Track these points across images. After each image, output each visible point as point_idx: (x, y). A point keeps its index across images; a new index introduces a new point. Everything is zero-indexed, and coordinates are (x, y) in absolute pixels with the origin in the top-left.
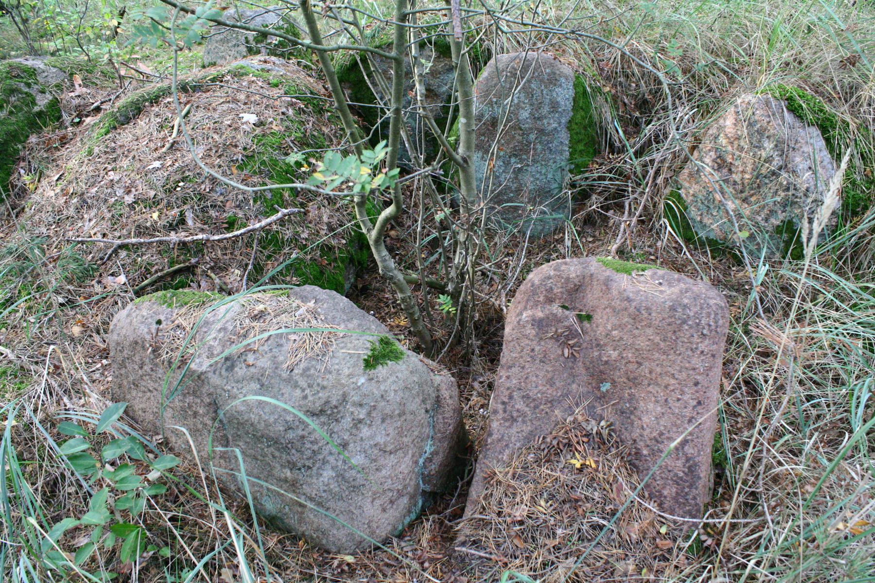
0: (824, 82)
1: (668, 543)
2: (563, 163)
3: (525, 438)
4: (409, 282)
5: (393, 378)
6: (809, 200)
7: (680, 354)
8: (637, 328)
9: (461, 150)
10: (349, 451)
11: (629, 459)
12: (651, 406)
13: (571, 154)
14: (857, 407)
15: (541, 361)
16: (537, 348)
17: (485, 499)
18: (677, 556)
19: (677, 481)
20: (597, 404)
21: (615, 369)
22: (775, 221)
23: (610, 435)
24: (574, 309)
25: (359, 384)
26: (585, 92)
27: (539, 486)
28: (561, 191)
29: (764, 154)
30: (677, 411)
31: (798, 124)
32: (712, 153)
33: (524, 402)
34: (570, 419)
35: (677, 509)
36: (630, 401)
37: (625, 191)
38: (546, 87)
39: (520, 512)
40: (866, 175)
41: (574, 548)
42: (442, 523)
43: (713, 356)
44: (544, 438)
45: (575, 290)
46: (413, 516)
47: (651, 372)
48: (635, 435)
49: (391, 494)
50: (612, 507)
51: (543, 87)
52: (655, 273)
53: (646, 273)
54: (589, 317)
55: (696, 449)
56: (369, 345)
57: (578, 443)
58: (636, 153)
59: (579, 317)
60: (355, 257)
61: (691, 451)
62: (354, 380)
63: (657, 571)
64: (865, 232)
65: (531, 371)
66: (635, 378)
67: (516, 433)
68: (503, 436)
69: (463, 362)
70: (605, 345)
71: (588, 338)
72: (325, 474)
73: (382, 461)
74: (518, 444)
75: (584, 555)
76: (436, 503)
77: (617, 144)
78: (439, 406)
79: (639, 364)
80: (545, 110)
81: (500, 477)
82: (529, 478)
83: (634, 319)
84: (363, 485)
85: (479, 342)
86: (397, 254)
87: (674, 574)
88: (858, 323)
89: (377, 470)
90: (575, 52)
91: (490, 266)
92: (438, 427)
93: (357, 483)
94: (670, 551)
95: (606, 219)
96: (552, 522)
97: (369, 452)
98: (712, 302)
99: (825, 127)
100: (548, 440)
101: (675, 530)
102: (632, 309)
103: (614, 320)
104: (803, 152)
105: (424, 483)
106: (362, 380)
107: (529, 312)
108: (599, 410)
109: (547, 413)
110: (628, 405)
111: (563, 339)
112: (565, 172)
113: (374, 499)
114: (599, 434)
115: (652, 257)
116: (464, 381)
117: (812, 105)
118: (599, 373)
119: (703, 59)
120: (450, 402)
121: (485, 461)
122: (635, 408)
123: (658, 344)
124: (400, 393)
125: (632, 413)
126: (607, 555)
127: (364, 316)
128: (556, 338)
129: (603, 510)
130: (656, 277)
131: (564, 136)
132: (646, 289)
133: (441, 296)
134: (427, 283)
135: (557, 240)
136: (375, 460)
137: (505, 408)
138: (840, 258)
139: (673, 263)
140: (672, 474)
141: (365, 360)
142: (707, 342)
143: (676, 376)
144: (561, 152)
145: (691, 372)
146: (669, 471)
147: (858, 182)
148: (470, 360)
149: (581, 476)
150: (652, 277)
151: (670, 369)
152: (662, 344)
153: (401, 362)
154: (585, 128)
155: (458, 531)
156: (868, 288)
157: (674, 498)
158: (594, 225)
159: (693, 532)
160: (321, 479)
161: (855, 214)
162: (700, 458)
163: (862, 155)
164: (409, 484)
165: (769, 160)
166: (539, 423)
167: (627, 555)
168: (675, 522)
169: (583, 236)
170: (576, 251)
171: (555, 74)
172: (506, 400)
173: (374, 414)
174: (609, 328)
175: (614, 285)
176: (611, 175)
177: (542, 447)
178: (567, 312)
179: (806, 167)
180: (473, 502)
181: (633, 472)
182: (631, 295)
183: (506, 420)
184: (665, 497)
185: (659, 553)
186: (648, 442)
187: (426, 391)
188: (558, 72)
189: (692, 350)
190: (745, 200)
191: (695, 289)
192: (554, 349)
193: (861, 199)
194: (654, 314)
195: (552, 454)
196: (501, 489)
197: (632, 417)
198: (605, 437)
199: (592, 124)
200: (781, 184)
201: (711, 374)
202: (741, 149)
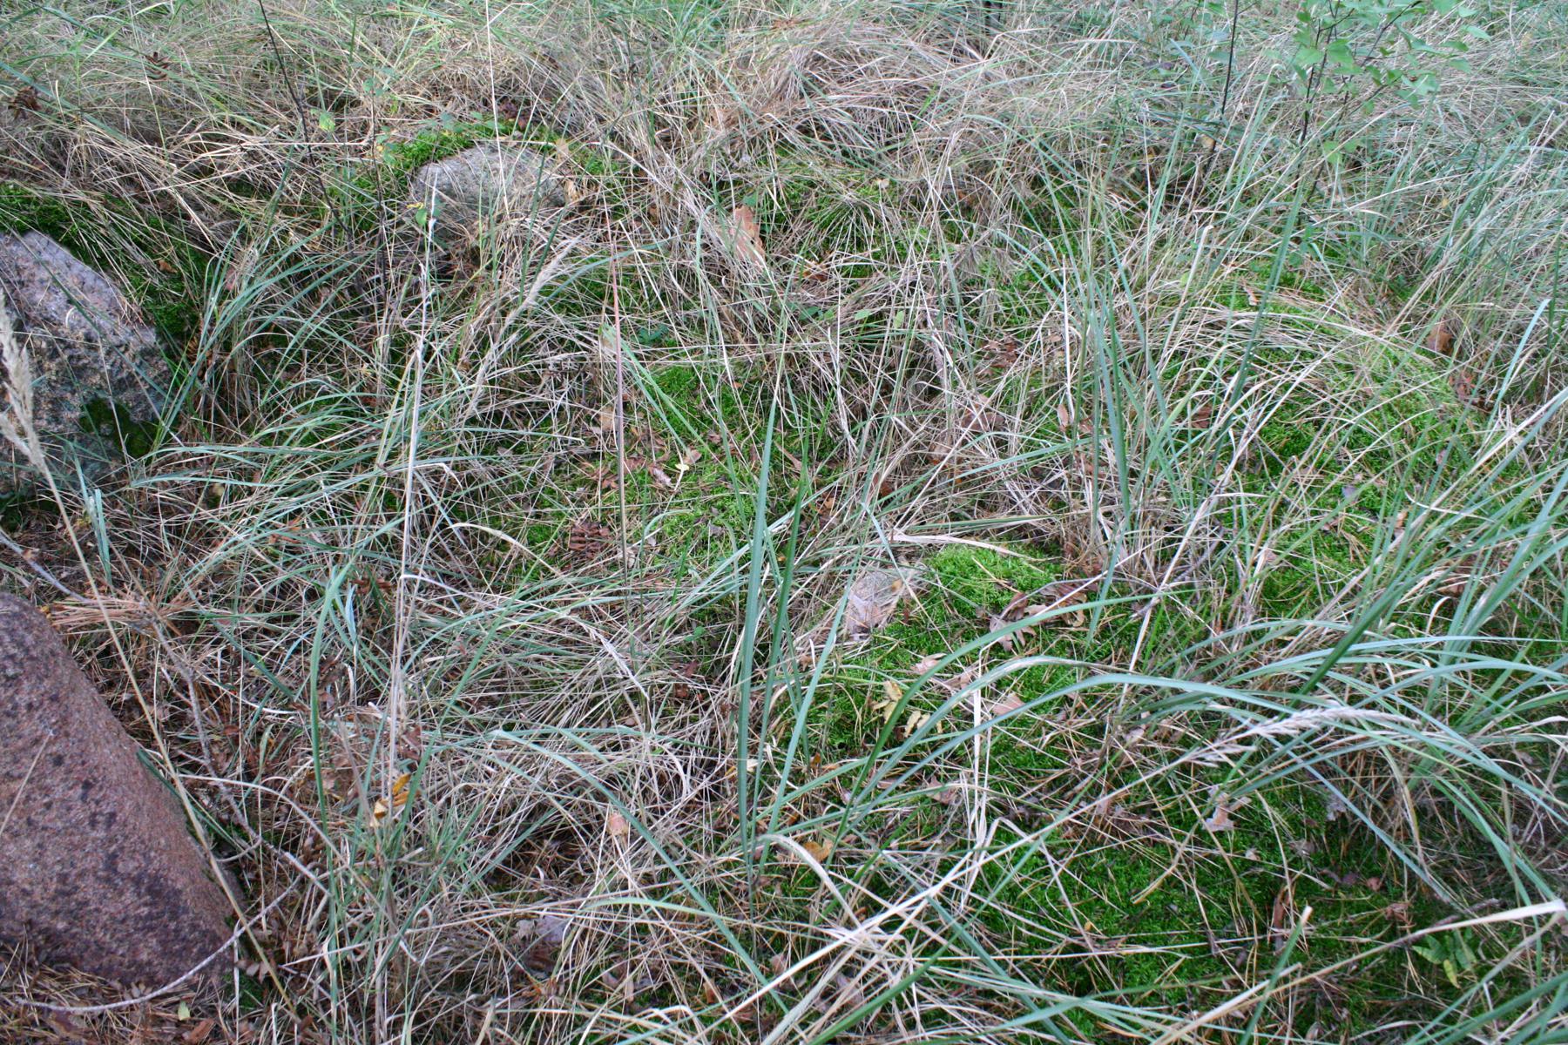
1: (206, 1024)
6: (102, 353)
11: (43, 957)
14: (1446, 297)
18: (234, 1030)
22: (72, 414)
30: (60, 824)
43: (54, 699)
48: (23, 912)
55: (137, 856)
61: (132, 865)
64: (216, 357)
99: (52, 223)
101: (202, 996)
104: (42, 281)
138: (207, 417)
140: (131, 923)
142: (26, 685)
143: (16, 773)
146: (123, 921)
147: (160, 287)
156: (271, 435)
157: (164, 954)
161: (183, 336)
162: (156, 864)
163: (139, 244)
168: (192, 986)
179: (62, 303)
181: (66, 971)
184: (149, 963)
186: (53, 907)
189: (8, 714)
193: (179, 311)
200: (39, 351)
201: (72, 729)
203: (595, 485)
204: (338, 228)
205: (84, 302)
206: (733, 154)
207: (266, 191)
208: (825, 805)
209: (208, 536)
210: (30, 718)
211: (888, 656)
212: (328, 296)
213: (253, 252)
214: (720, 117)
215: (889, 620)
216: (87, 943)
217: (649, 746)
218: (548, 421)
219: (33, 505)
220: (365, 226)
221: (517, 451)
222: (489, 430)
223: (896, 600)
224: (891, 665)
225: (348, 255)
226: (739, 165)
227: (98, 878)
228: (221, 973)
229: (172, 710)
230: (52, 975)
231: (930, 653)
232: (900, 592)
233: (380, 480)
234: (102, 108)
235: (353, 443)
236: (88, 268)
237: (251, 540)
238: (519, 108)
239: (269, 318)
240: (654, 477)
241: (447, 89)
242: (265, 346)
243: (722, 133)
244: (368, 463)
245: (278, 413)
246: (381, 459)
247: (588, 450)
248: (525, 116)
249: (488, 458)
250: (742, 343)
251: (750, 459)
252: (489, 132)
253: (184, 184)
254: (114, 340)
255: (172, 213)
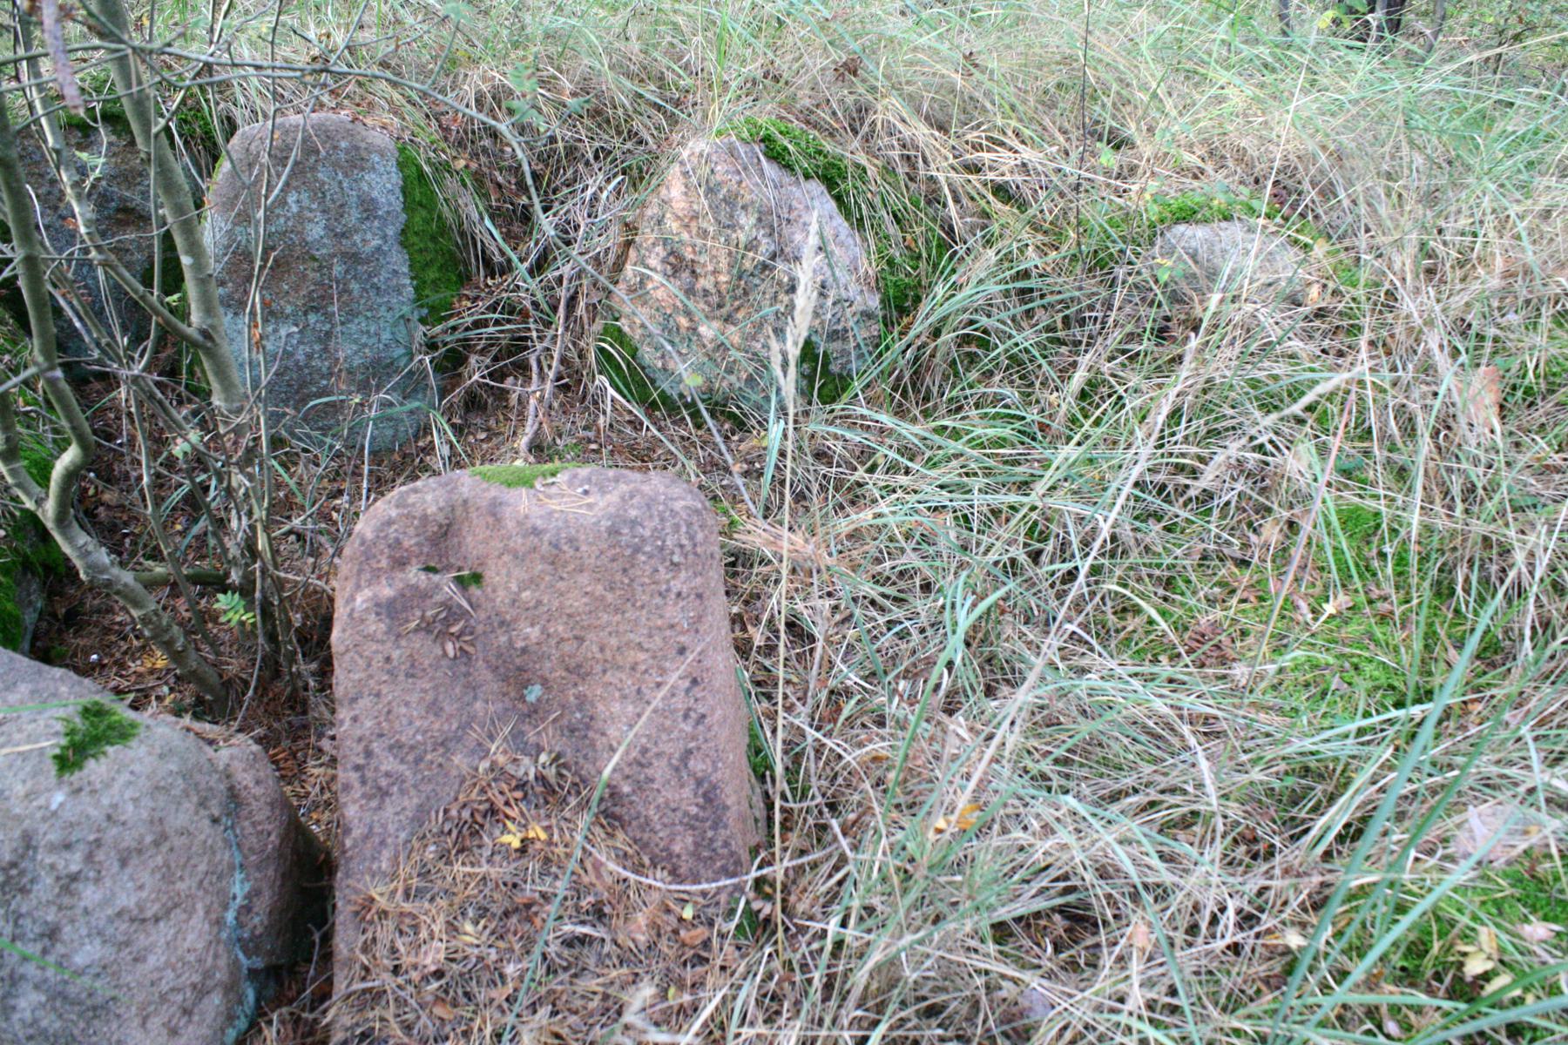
0: (818, 106)
1: (701, 932)
2: (406, 309)
3: (412, 820)
4: (151, 585)
5: (125, 777)
7: (642, 607)
8: (562, 578)
9: (195, 317)
10: (63, 942)
12: (616, 707)
13: (416, 289)
15: (408, 675)
16: (395, 654)
17: (365, 950)
19: (691, 823)
20: (526, 728)
21: (541, 658)
23: (560, 775)
24: (448, 568)
25: (54, 807)
26: (421, 175)
27: (457, 900)
28: (411, 359)
29: (743, 238)
31: (787, 179)
32: (659, 249)
33: (395, 757)
34: (484, 765)
35: (702, 871)
36: (580, 708)
37: (526, 339)
38: (346, 175)
39: (432, 957)
40: (908, 248)
41: (543, 990)
42: (297, 1020)
43: (699, 596)
44: (446, 811)
45: (441, 538)
46: (242, 1024)
47: (602, 650)
49: (180, 997)
50: (591, 899)
51: (340, 177)
52: (575, 476)
53: (560, 478)
54: (477, 578)
56: (59, 727)
57: (507, 803)
58: (531, 272)
59: (459, 581)
60: (34, 559)
61: (701, 766)
62: (41, 801)
63: (693, 985)
64: (923, 338)
65: (394, 698)
66: (579, 666)
67: (394, 815)
68: (371, 828)
69: (292, 708)
70: (515, 620)
71: (483, 615)
72: (22, 1003)
73: (142, 941)
74: (403, 835)
75: (564, 998)
76: (282, 985)
77: (497, 258)
78: (238, 805)
79: (580, 639)
80: (353, 216)
81: (382, 902)
82: (436, 890)
83: (553, 563)
84: (114, 999)
85: (314, 666)
86: (126, 535)
87: (721, 981)
88: (942, 487)
89: (136, 960)
90: (390, 102)
91: (304, 523)
92: (247, 845)
93: (99, 1000)
94: (706, 944)
95: (503, 395)
96: (493, 955)
97: (110, 930)
98: (678, 505)
99: (831, 176)
100: (454, 813)
102: (545, 548)
103: (520, 573)
105: (248, 955)
106: (59, 798)
107: (367, 593)
108: (531, 736)
109: (440, 765)
110: (578, 715)
111: (438, 626)
112: (412, 325)
113: (145, 1020)
114: (541, 778)
115: (594, 446)
116: (301, 743)
117: (803, 144)
118: (516, 673)
119: (619, 89)
120: (258, 791)
121: (350, 882)
122: (592, 718)
123: (603, 598)
124: (147, 802)
125: (588, 727)
126: (603, 985)
127: (40, 672)
128: (426, 627)
129: (578, 909)
130: (577, 482)
131: (398, 260)
132: (562, 507)
133: (220, 596)
134: (188, 578)
135: (423, 449)
136: (127, 944)
137: (363, 776)
138: (895, 389)
139: (632, 448)
140: (679, 814)
141: (55, 757)
142: (683, 575)
143: (646, 646)
144: (398, 290)
145: (668, 633)
146: (674, 810)
147: (898, 260)
148: (305, 702)
149: (524, 861)
150: (570, 484)
151: (632, 636)
152: (610, 597)
153: (134, 743)
154: (433, 239)
155: (327, 1025)
156: (945, 428)
158: (481, 411)
159: (737, 901)
160: (16, 1017)
161: (903, 311)
162: (719, 775)
163: (895, 216)
164: (215, 967)
165: (752, 246)
166: (430, 787)
167: (637, 975)
168: (704, 894)
169: (469, 433)
170: (455, 462)
171: (357, 148)
172: (361, 761)
173: (100, 856)
174: (514, 588)
175: (507, 512)
176: (496, 316)
177: (446, 829)
178: (436, 578)
180: (344, 964)
181: (614, 828)
182: (539, 522)
183: (368, 797)
184: (678, 856)
185: (689, 953)
186: (627, 771)
187: (203, 786)
188: (363, 145)
190: (728, 319)
191: (646, 488)
192: (425, 647)
193: (907, 286)
194: (584, 548)
195: (467, 834)
196: (390, 924)
197: (591, 734)
198: (553, 781)
199: (444, 230)
200: (780, 283)
202: (704, 234)
203: (1233, 591)
204: (1074, 258)
205: (832, 252)
206: (1500, 309)
207: (1023, 206)
208: (1362, 1022)
209: (856, 497)
210: (676, 604)
211: (1495, 901)
212: (1043, 318)
213: (991, 255)
214: (1499, 265)
215: (1509, 863)
216: (639, 813)
217: (1207, 877)
218: (1209, 512)
219: (723, 412)
220: (1101, 264)
221: (1168, 529)
222: (1150, 498)
223: (1523, 846)
224: (1494, 911)
225: (1070, 285)
226: (1503, 322)
227: (670, 764)
228: (731, 895)
229: (768, 639)
230: (602, 826)
231: (1545, 919)
232: (1535, 839)
233: (1033, 508)
234: (908, 89)
235: (1017, 463)
236: (846, 224)
237: (899, 518)
238: (1288, 197)
239: (984, 321)
240: (1296, 608)
241: (1223, 157)
242: (968, 343)
243: (1495, 282)
244: (1024, 486)
245: (960, 409)
246: (1040, 487)
247: (1238, 555)
248: (1293, 207)
249: (1137, 524)
250: (1438, 508)
251: (1403, 627)
252: (1252, 211)
253: (953, 175)
254: (844, 295)
255: (934, 198)
